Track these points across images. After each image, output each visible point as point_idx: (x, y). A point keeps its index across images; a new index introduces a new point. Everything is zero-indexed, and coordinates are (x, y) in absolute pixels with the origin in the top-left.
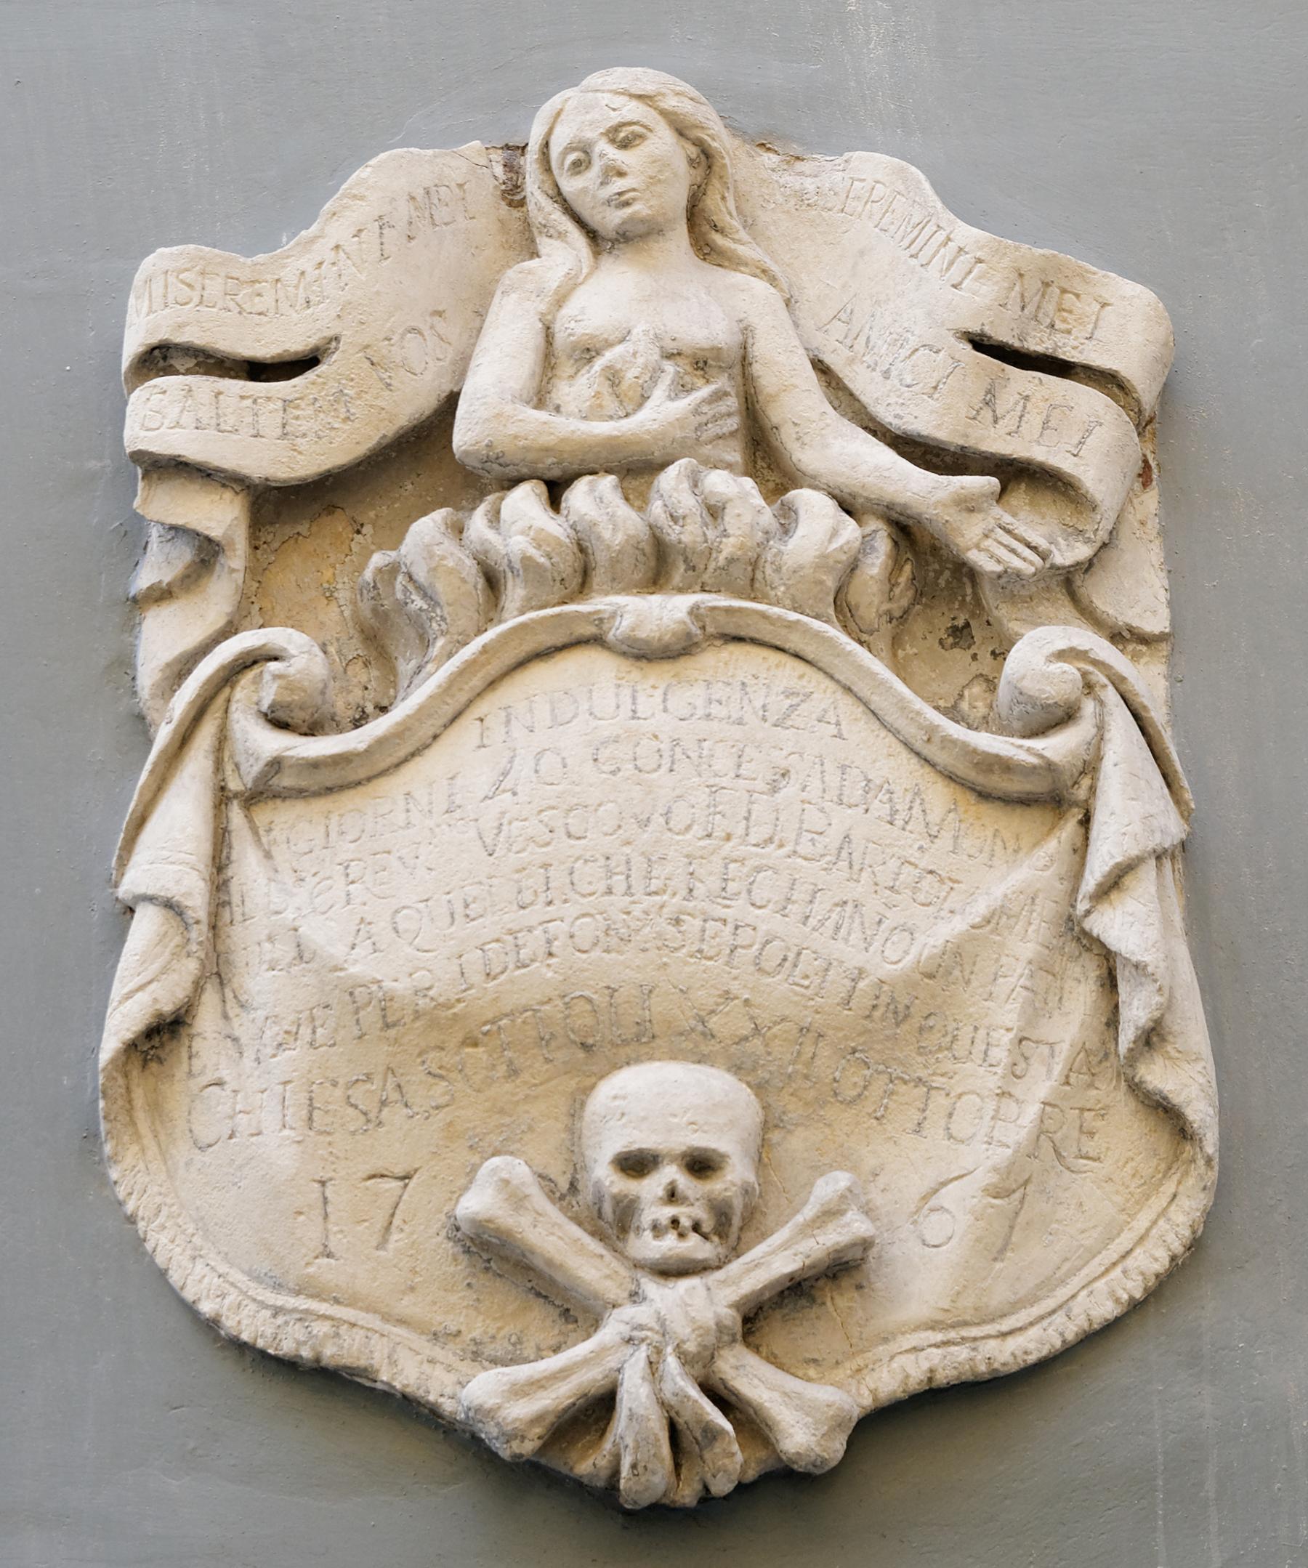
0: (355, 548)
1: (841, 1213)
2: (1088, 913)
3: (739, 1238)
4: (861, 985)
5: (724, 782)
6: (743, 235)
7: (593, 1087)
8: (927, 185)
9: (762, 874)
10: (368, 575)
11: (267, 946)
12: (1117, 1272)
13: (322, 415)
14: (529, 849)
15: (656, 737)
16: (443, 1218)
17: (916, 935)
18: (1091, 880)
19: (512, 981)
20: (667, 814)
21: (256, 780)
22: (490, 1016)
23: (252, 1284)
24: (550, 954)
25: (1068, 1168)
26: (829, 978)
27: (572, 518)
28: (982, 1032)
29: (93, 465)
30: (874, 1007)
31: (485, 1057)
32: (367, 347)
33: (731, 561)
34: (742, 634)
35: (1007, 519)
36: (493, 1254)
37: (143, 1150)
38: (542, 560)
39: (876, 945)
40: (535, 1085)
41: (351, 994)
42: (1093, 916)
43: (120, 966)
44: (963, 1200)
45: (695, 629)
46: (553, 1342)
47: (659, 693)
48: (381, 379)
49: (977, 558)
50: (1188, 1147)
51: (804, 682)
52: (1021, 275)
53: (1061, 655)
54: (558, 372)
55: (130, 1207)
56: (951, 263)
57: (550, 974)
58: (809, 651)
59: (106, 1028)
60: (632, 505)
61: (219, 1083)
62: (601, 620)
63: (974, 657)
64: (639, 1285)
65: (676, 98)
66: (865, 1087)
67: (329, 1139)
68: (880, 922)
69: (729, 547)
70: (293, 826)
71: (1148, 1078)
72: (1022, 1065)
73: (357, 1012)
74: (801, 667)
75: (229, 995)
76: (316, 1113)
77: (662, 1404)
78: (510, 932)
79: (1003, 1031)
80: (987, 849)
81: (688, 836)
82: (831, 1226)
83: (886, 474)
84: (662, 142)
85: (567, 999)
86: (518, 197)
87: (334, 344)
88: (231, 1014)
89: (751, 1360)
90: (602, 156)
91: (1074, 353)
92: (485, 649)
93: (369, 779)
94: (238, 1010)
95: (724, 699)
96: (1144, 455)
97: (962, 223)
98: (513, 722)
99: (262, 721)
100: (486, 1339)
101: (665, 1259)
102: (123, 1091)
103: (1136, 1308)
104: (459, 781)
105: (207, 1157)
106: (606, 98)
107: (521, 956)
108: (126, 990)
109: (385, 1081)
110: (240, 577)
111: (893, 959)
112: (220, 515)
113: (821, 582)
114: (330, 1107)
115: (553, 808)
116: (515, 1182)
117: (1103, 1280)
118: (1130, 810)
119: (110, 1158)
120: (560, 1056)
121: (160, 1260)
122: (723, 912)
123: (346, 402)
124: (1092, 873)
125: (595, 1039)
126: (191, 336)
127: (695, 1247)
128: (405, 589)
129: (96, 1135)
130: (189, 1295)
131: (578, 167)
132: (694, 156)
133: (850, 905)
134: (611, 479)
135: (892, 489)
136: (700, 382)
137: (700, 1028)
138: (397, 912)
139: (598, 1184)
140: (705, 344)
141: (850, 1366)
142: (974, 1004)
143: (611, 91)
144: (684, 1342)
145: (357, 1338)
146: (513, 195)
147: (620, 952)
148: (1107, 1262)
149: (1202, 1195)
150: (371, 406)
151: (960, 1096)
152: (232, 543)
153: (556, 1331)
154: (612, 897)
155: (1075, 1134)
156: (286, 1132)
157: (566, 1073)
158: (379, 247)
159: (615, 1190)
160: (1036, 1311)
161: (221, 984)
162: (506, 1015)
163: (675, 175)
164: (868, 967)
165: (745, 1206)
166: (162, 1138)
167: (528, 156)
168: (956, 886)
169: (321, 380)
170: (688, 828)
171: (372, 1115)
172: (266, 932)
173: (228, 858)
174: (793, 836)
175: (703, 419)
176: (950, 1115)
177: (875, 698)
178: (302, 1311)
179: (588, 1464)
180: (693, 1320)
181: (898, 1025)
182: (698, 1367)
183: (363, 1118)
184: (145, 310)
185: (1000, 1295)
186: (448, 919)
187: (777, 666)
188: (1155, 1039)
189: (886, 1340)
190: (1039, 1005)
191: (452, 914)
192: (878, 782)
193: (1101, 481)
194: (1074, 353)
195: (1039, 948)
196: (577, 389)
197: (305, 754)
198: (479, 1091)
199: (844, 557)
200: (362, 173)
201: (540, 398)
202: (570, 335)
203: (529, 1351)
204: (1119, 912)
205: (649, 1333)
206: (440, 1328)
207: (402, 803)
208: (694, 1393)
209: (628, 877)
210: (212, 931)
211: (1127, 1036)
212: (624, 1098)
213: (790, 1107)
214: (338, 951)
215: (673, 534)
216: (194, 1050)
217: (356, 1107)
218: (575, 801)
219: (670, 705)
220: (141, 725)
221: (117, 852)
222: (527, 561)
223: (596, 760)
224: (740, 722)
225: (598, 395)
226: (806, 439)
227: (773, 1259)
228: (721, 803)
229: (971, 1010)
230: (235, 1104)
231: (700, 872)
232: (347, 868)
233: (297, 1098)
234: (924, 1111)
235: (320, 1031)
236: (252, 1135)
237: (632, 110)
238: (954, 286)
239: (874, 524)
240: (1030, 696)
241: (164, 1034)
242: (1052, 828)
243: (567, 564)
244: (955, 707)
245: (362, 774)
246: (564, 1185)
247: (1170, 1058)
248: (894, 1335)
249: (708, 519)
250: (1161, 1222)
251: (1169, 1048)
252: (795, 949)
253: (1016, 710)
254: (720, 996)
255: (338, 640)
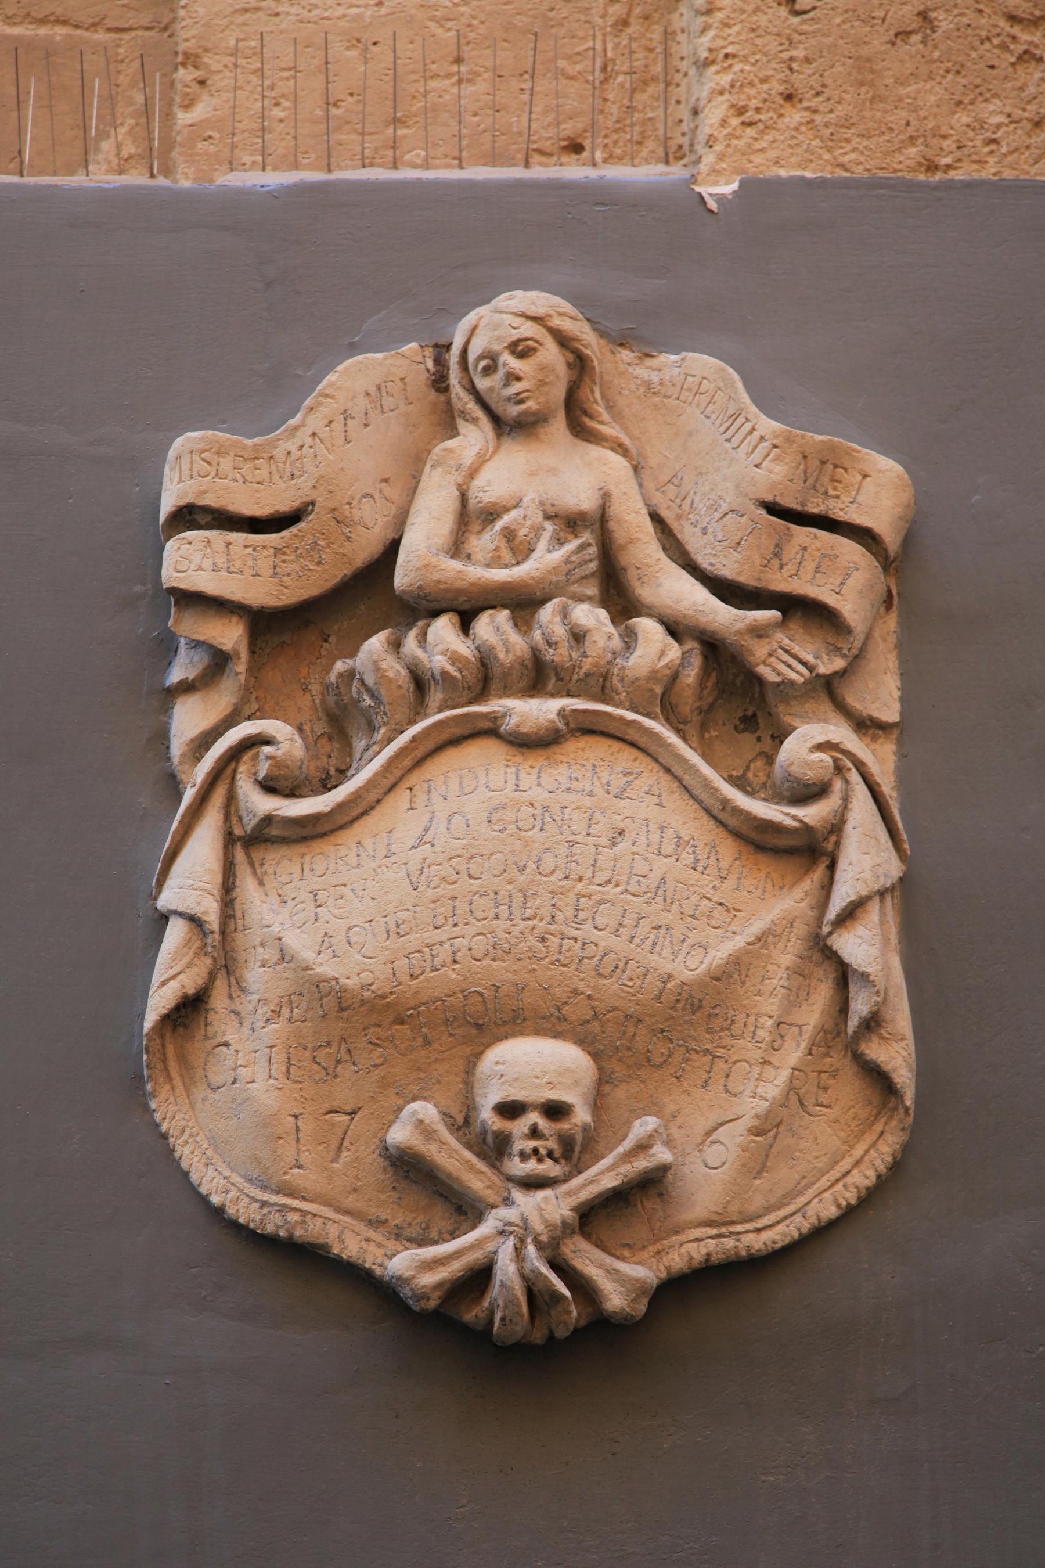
0: (323, 653)
1: (650, 1146)
2: (830, 934)
3: (579, 1158)
4: (669, 986)
5: (578, 838)
6: (606, 416)
7: (482, 1053)
8: (740, 385)
9: (603, 906)
10: (333, 677)
11: (260, 950)
12: (839, 1186)
13: (302, 560)
14: (442, 886)
15: (532, 805)
16: (376, 1140)
17: (709, 950)
18: (832, 913)
19: (427, 980)
20: (538, 862)
21: (253, 829)
22: (412, 1004)
23: (247, 1185)
24: (455, 962)
25: (808, 1113)
26: (647, 981)
27: (478, 642)
28: (752, 1018)
29: (138, 588)
30: (678, 1001)
31: (409, 1032)
32: (335, 509)
33: (588, 675)
34: (595, 728)
35: (786, 642)
36: (409, 1168)
37: (173, 1089)
38: (457, 674)
39: (681, 957)
40: (442, 1052)
41: (317, 986)
42: (834, 936)
43: (158, 960)
44: (733, 1139)
45: (561, 726)
46: (450, 1228)
47: (535, 771)
48: (343, 534)
49: (763, 670)
50: (893, 1099)
51: (636, 764)
52: (805, 457)
53: (820, 747)
54: (470, 528)
55: (164, 1128)
56: (755, 447)
57: (454, 976)
58: (642, 741)
59: (149, 1005)
60: (520, 630)
61: (226, 1045)
62: (496, 718)
63: (759, 739)
64: (510, 1193)
65: (560, 318)
66: (669, 1056)
67: (300, 1086)
68: (684, 941)
69: (587, 664)
70: (278, 863)
71: (867, 1052)
72: (779, 1041)
73: (321, 999)
74: (635, 753)
75: (233, 981)
76: (292, 1068)
77: (523, 1277)
78: (427, 946)
79: (766, 1018)
80: (761, 886)
81: (552, 879)
82: (642, 1156)
83: (701, 608)
84: (550, 353)
85: (466, 993)
86: (444, 385)
87: (310, 508)
88: (234, 996)
89: (583, 1244)
90: (505, 365)
91: (841, 513)
92: (414, 739)
93: (332, 831)
94: (239, 993)
95: (580, 777)
96: (888, 587)
97: (764, 417)
98: (433, 791)
99: (257, 787)
100: (405, 1225)
101: (528, 1176)
102: (159, 1047)
103: (849, 1213)
104: (395, 835)
105: (217, 1096)
106: (508, 319)
107: (435, 963)
108: (163, 979)
109: (340, 1047)
110: (242, 678)
111: (691, 966)
112: (230, 635)
113: (651, 690)
114: (301, 1064)
115: (459, 856)
116: (427, 1121)
117: (830, 1192)
118: (866, 860)
119: (150, 1094)
120: (459, 1032)
121: (184, 1165)
122: (574, 933)
123: (319, 550)
124: (834, 906)
125: (486, 1019)
126: (209, 500)
127: (549, 1168)
128: (359, 692)
129: (142, 1076)
130: (203, 1190)
131: (488, 371)
132: (571, 361)
133: (664, 928)
134: (506, 613)
135: (705, 620)
136: (570, 537)
137: (557, 1014)
138: (350, 929)
139: (483, 1122)
140: (576, 509)
141: (652, 1249)
142: (748, 998)
143: (512, 313)
144: (539, 1235)
145: (318, 1224)
146: (439, 382)
147: (504, 961)
148: (833, 1179)
149: (901, 1134)
150: (337, 553)
151: (735, 1063)
152: (237, 655)
153: (452, 1221)
154: (499, 922)
155: (815, 1089)
156: (272, 1081)
157: (463, 1044)
158: (343, 434)
159: (495, 1128)
160: (782, 1213)
161: (228, 973)
162: (424, 1004)
163: (557, 377)
164: (675, 973)
165: (584, 1138)
166: (187, 1080)
167: (452, 352)
168: (737, 913)
169: (300, 534)
170: (553, 872)
171: (330, 1071)
172: (259, 939)
173: (233, 883)
174: (625, 878)
175: (572, 566)
176: (727, 1076)
177: (686, 777)
178: (280, 1205)
179: (471, 1315)
180: (546, 1221)
181: (693, 1013)
182: (548, 1251)
183: (324, 1072)
184: (176, 479)
185: (758, 1202)
186: (386, 936)
187: (618, 752)
188: (873, 1024)
189: (677, 1233)
190: (795, 998)
191: (388, 932)
192: (686, 839)
193: (855, 612)
194: (841, 513)
195: (794, 958)
196: (484, 542)
197: (287, 814)
198: (404, 1055)
199: (668, 672)
200: (331, 377)
201: (457, 548)
202: (479, 502)
203: (434, 1234)
204: (852, 935)
205: (516, 1229)
206: (374, 1217)
207: (355, 849)
208: (545, 1270)
209: (510, 907)
210: (221, 943)
211: (853, 1023)
212: (504, 1064)
213: (617, 1069)
214: (308, 956)
215: (549, 655)
216: (209, 1020)
217: (319, 1064)
218: (475, 851)
219: (543, 781)
220: (173, 786)
221: (156, 877)
222: (444, 674)
223: (489, 822)
224: (591, 795)
225: (497, 549)
226: (645, 579)
227: (603, 1175)
228: (576, 854)
229: (745, 1002)
230: (237, 1059)
231: (560, 904)
232: (316, 895)
233: (279, 1057)
234: (709, 1072)
235: (295, 1011)
236: (248, 1083)
237: (528, 329)
238: (756, 466)
239: (691, 644)
240: (796, 778)
241: (190, 1009)
242: (807, 872)
243: (472, 676)
244: (743, 776)
245: (327, 828)
246: (460, 1120)
247: (884, 1038)
248: (683, 1229)
249: (573, 643)
250: (872, 1152)
251: (883, 1031)
252: (624, 960)
253: (787, 784)
254: (571, 992)
255: (311, 721)
